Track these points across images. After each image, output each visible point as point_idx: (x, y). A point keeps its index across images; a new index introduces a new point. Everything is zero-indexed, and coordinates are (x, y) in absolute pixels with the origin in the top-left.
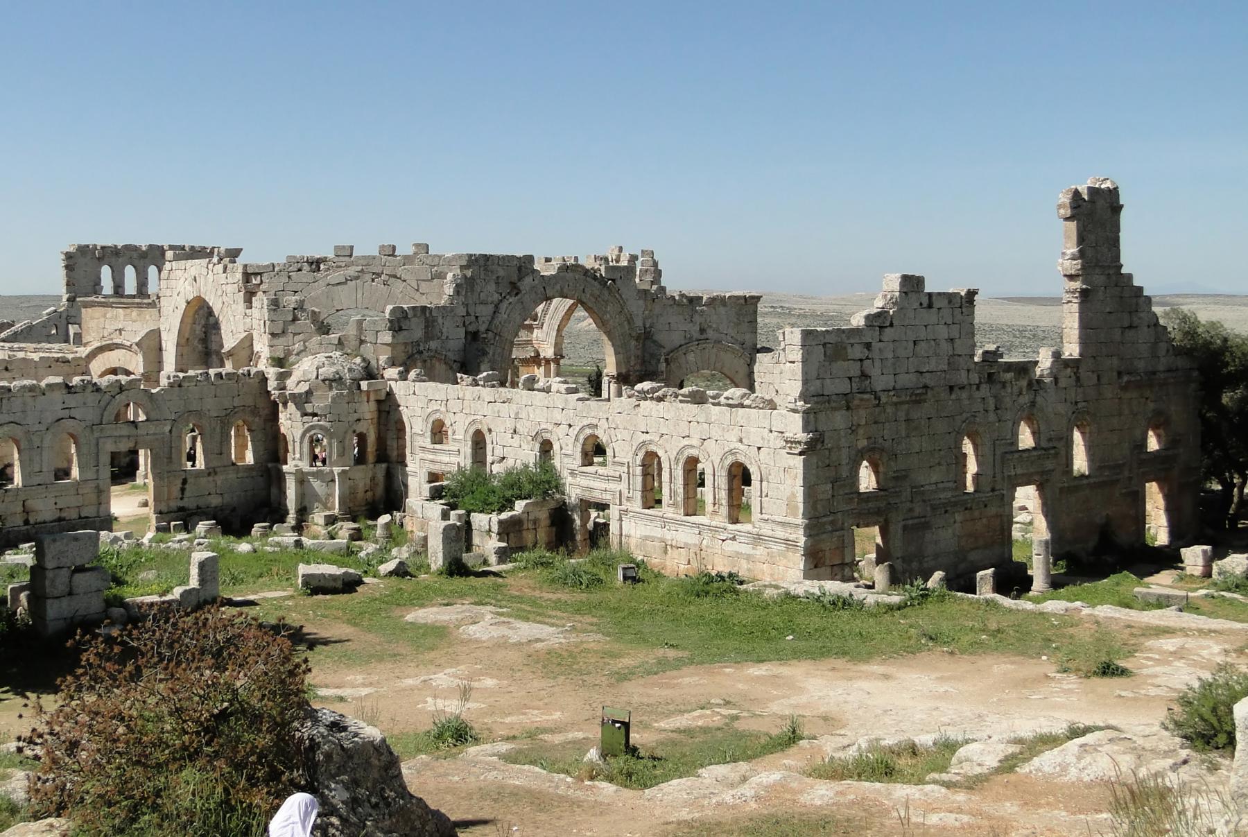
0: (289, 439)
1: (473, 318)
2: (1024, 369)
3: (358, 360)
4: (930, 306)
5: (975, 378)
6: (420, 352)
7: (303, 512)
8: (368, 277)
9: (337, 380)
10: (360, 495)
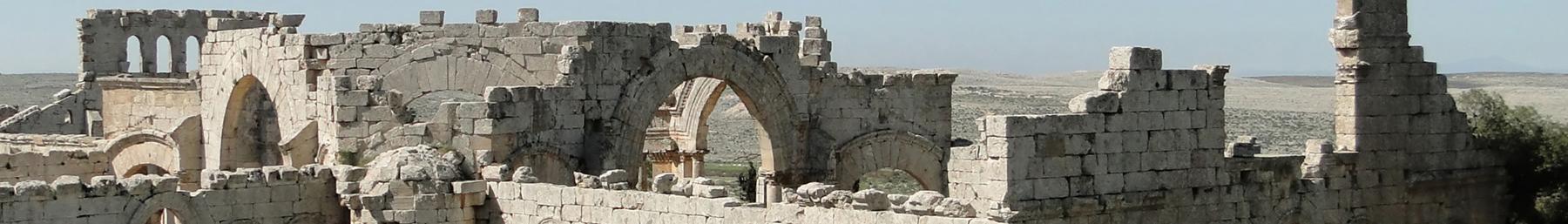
1: (594, 103)
2: (1286, 167)
3: (450, 155)
4: (1168, 87)
5: (1225, 178)
6: (528, 146)
8: (463, 51)
9: (423, 181)
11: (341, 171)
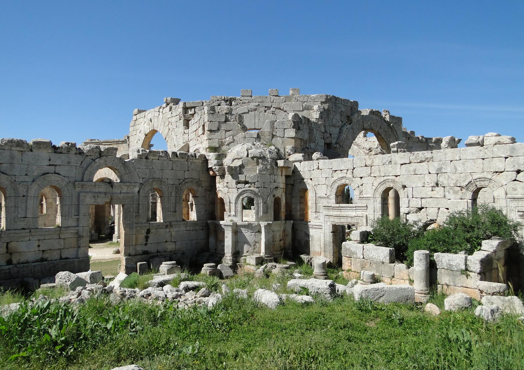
0: (226, 201)
1: (328, 135)
3: (273, 148)
7: (237, 254)
8: (263, 109)
9: (260, 159)
10: (277, 243)
11: (212, 157)
